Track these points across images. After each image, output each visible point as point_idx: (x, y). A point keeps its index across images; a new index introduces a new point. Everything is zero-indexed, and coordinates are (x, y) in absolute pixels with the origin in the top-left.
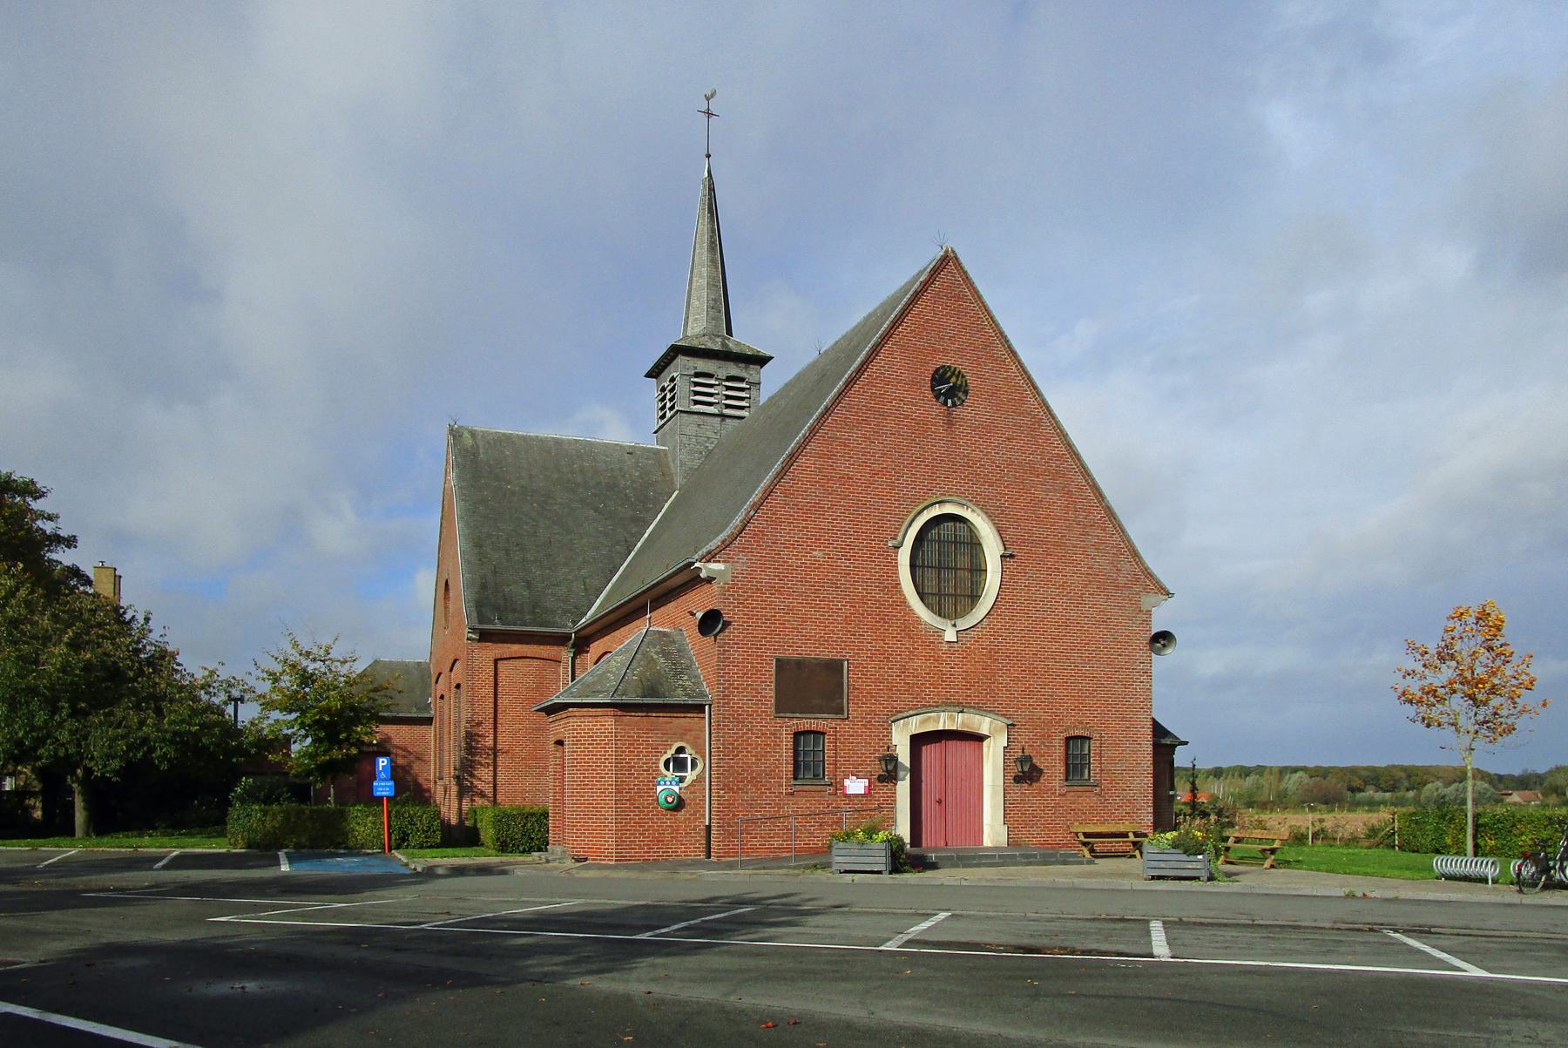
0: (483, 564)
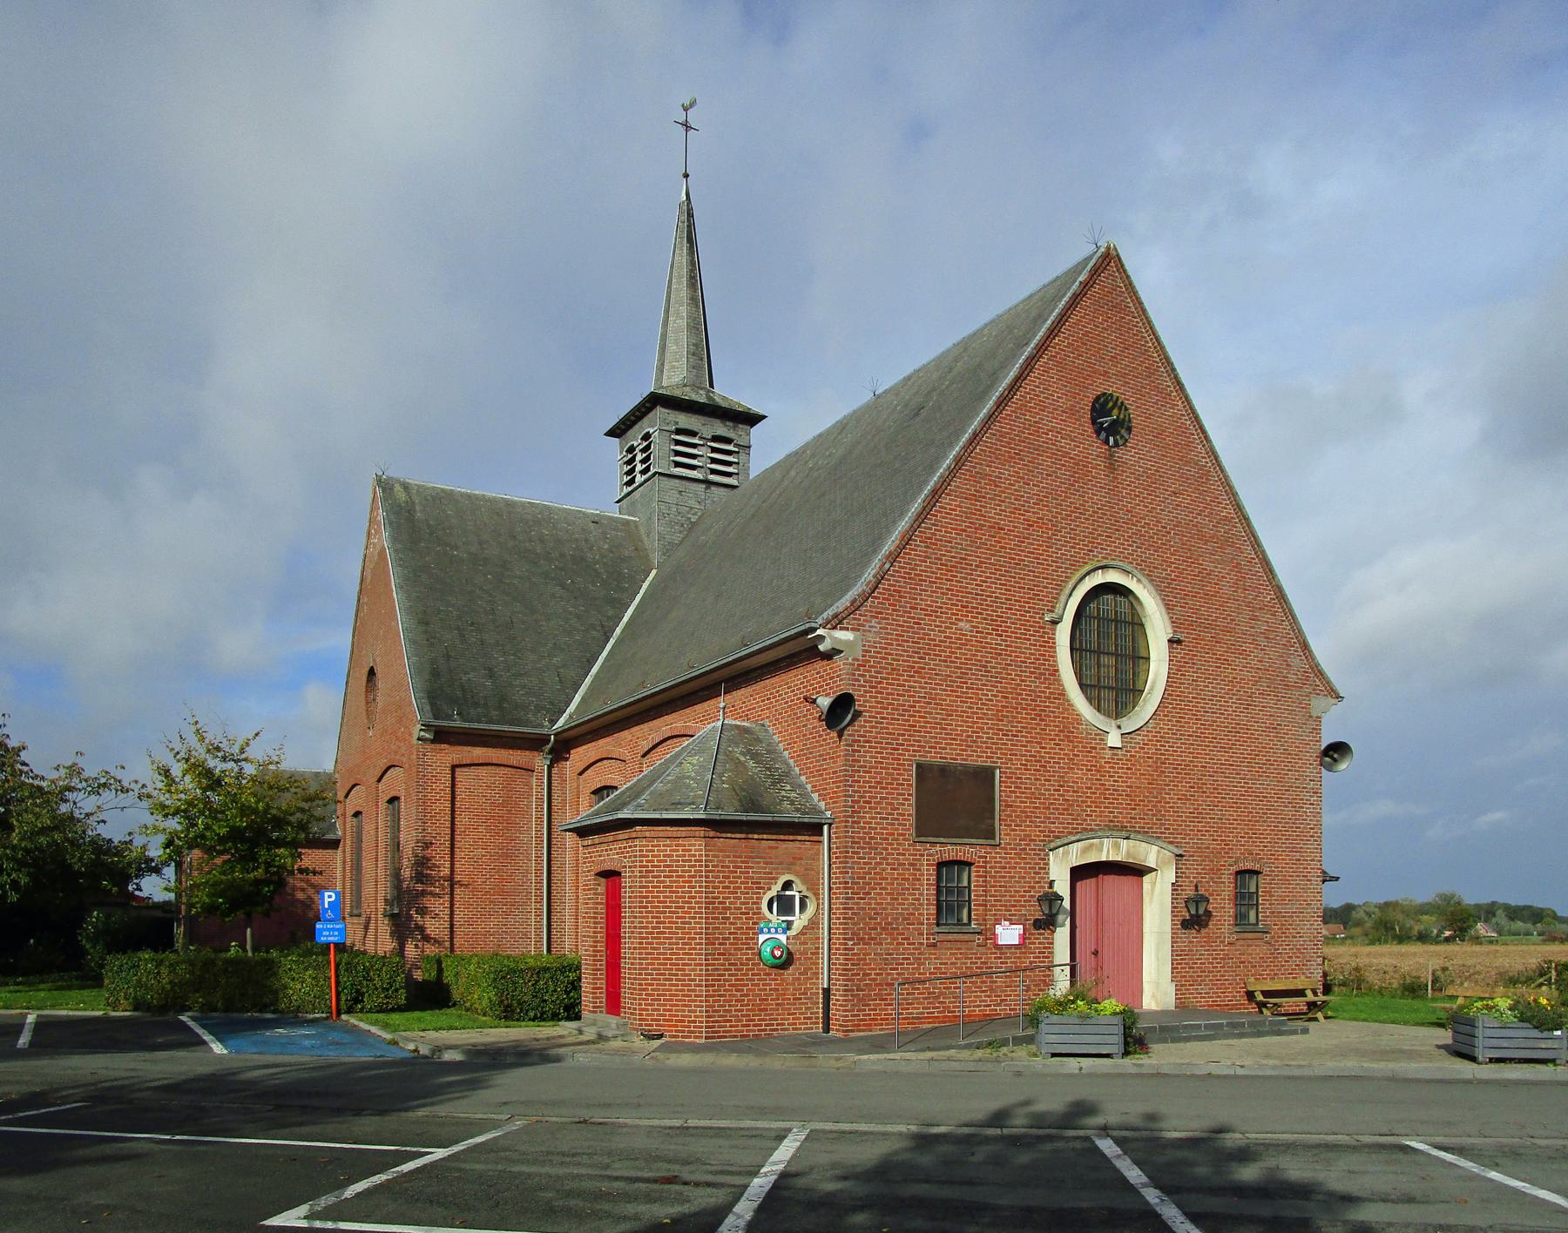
0: (432, 645)
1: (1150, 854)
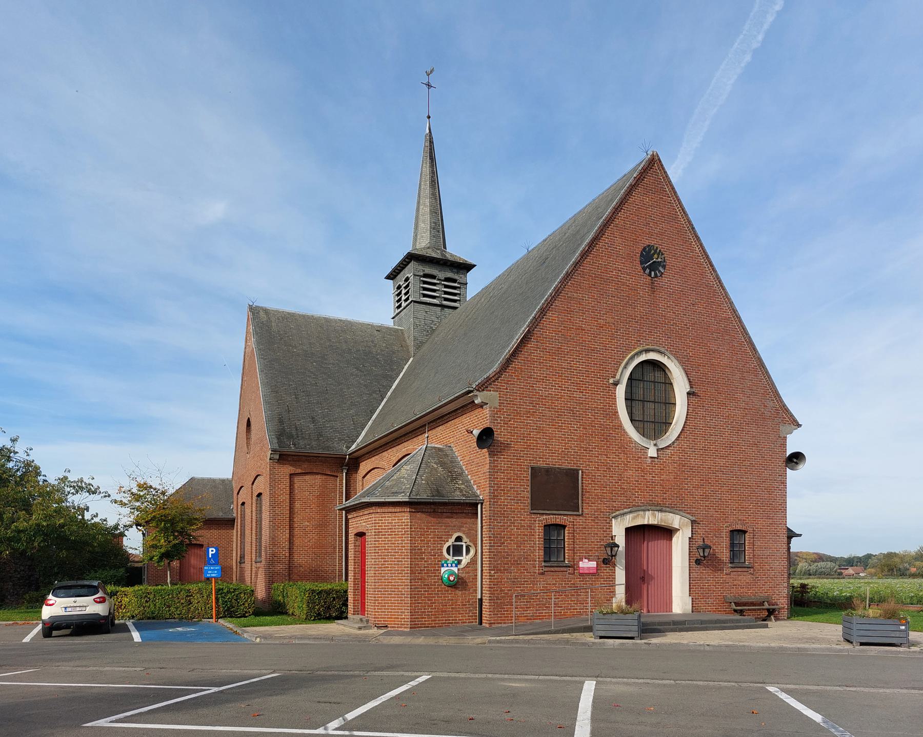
1: (674, 520)
